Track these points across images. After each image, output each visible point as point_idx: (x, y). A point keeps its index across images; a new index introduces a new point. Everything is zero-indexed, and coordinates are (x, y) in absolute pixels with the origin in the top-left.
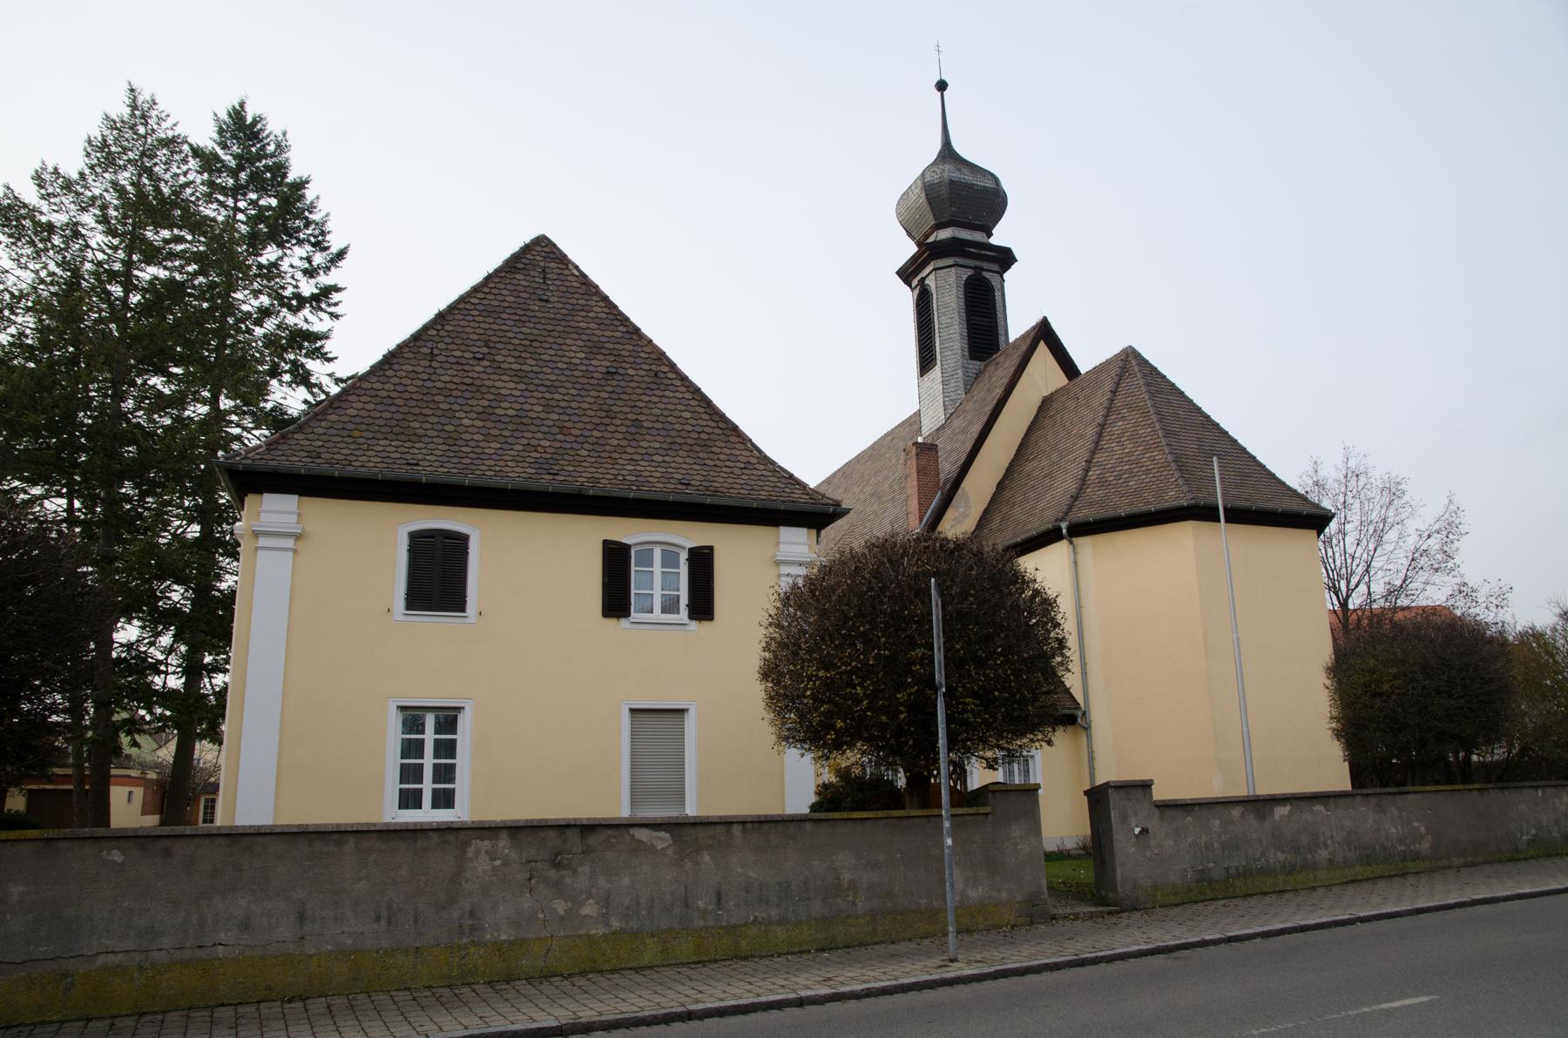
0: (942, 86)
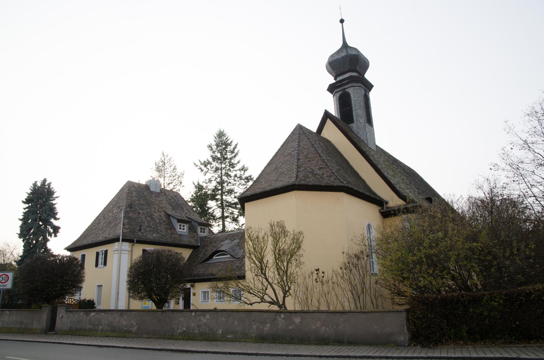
0: (342, 21)
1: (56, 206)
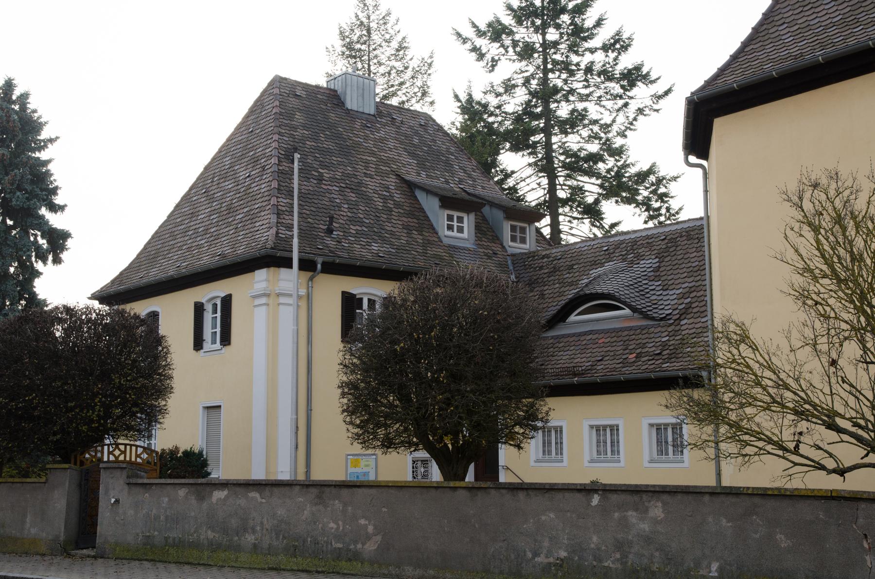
1: (50, 167)
